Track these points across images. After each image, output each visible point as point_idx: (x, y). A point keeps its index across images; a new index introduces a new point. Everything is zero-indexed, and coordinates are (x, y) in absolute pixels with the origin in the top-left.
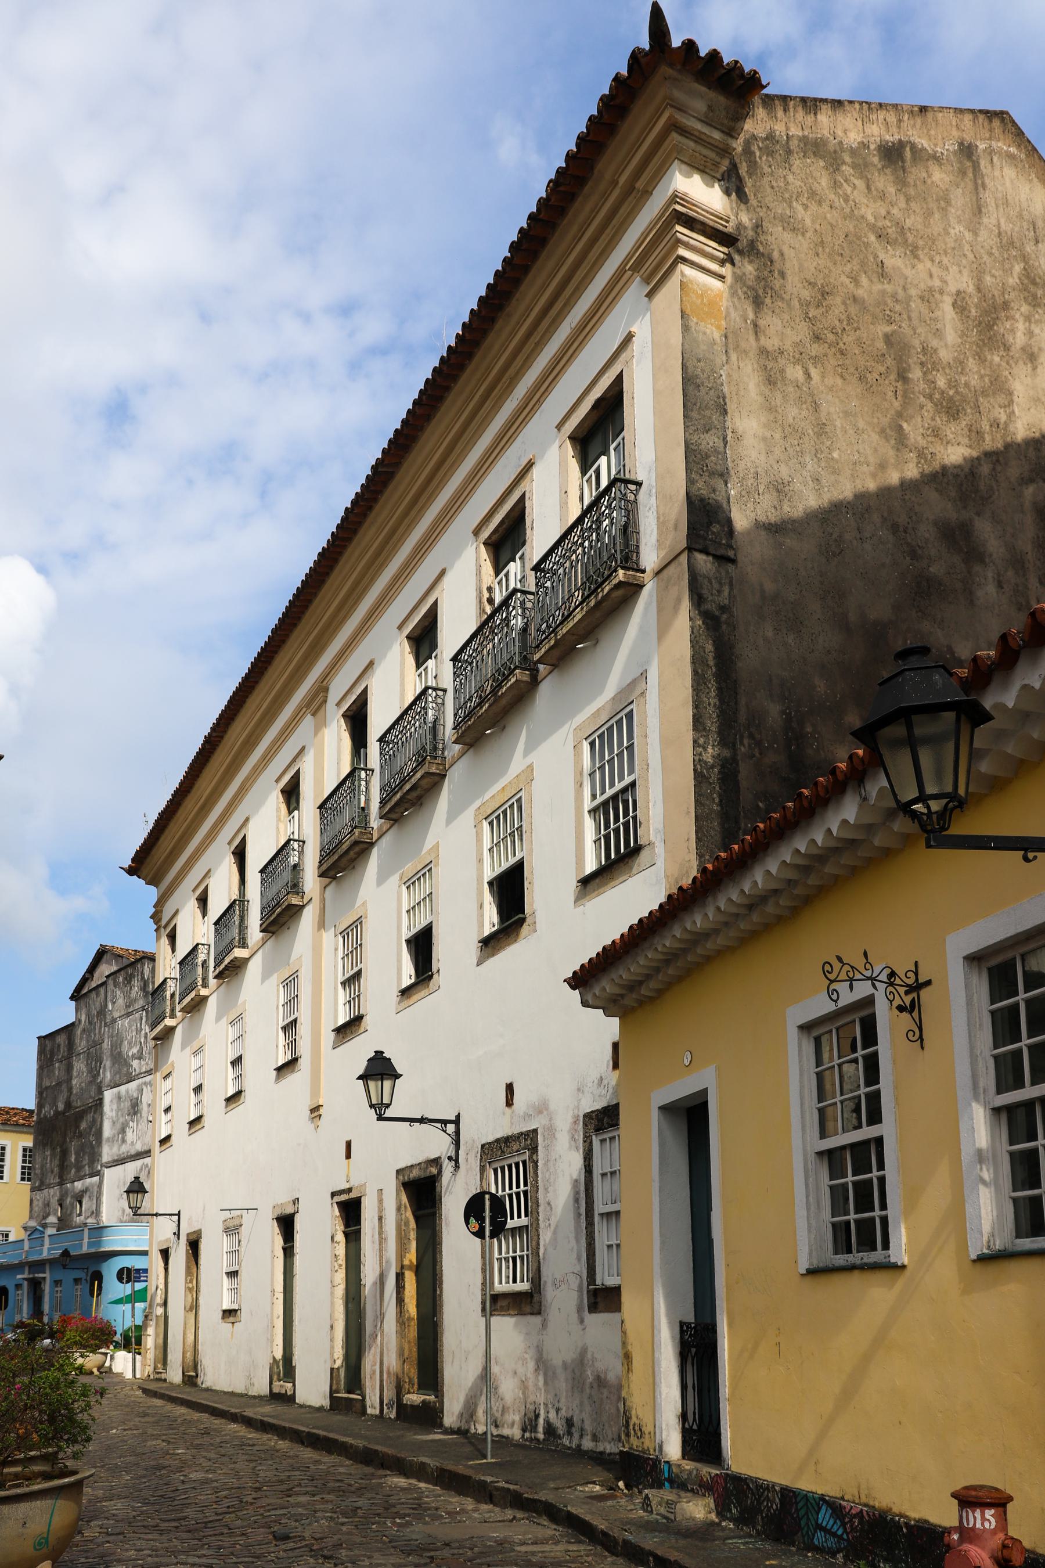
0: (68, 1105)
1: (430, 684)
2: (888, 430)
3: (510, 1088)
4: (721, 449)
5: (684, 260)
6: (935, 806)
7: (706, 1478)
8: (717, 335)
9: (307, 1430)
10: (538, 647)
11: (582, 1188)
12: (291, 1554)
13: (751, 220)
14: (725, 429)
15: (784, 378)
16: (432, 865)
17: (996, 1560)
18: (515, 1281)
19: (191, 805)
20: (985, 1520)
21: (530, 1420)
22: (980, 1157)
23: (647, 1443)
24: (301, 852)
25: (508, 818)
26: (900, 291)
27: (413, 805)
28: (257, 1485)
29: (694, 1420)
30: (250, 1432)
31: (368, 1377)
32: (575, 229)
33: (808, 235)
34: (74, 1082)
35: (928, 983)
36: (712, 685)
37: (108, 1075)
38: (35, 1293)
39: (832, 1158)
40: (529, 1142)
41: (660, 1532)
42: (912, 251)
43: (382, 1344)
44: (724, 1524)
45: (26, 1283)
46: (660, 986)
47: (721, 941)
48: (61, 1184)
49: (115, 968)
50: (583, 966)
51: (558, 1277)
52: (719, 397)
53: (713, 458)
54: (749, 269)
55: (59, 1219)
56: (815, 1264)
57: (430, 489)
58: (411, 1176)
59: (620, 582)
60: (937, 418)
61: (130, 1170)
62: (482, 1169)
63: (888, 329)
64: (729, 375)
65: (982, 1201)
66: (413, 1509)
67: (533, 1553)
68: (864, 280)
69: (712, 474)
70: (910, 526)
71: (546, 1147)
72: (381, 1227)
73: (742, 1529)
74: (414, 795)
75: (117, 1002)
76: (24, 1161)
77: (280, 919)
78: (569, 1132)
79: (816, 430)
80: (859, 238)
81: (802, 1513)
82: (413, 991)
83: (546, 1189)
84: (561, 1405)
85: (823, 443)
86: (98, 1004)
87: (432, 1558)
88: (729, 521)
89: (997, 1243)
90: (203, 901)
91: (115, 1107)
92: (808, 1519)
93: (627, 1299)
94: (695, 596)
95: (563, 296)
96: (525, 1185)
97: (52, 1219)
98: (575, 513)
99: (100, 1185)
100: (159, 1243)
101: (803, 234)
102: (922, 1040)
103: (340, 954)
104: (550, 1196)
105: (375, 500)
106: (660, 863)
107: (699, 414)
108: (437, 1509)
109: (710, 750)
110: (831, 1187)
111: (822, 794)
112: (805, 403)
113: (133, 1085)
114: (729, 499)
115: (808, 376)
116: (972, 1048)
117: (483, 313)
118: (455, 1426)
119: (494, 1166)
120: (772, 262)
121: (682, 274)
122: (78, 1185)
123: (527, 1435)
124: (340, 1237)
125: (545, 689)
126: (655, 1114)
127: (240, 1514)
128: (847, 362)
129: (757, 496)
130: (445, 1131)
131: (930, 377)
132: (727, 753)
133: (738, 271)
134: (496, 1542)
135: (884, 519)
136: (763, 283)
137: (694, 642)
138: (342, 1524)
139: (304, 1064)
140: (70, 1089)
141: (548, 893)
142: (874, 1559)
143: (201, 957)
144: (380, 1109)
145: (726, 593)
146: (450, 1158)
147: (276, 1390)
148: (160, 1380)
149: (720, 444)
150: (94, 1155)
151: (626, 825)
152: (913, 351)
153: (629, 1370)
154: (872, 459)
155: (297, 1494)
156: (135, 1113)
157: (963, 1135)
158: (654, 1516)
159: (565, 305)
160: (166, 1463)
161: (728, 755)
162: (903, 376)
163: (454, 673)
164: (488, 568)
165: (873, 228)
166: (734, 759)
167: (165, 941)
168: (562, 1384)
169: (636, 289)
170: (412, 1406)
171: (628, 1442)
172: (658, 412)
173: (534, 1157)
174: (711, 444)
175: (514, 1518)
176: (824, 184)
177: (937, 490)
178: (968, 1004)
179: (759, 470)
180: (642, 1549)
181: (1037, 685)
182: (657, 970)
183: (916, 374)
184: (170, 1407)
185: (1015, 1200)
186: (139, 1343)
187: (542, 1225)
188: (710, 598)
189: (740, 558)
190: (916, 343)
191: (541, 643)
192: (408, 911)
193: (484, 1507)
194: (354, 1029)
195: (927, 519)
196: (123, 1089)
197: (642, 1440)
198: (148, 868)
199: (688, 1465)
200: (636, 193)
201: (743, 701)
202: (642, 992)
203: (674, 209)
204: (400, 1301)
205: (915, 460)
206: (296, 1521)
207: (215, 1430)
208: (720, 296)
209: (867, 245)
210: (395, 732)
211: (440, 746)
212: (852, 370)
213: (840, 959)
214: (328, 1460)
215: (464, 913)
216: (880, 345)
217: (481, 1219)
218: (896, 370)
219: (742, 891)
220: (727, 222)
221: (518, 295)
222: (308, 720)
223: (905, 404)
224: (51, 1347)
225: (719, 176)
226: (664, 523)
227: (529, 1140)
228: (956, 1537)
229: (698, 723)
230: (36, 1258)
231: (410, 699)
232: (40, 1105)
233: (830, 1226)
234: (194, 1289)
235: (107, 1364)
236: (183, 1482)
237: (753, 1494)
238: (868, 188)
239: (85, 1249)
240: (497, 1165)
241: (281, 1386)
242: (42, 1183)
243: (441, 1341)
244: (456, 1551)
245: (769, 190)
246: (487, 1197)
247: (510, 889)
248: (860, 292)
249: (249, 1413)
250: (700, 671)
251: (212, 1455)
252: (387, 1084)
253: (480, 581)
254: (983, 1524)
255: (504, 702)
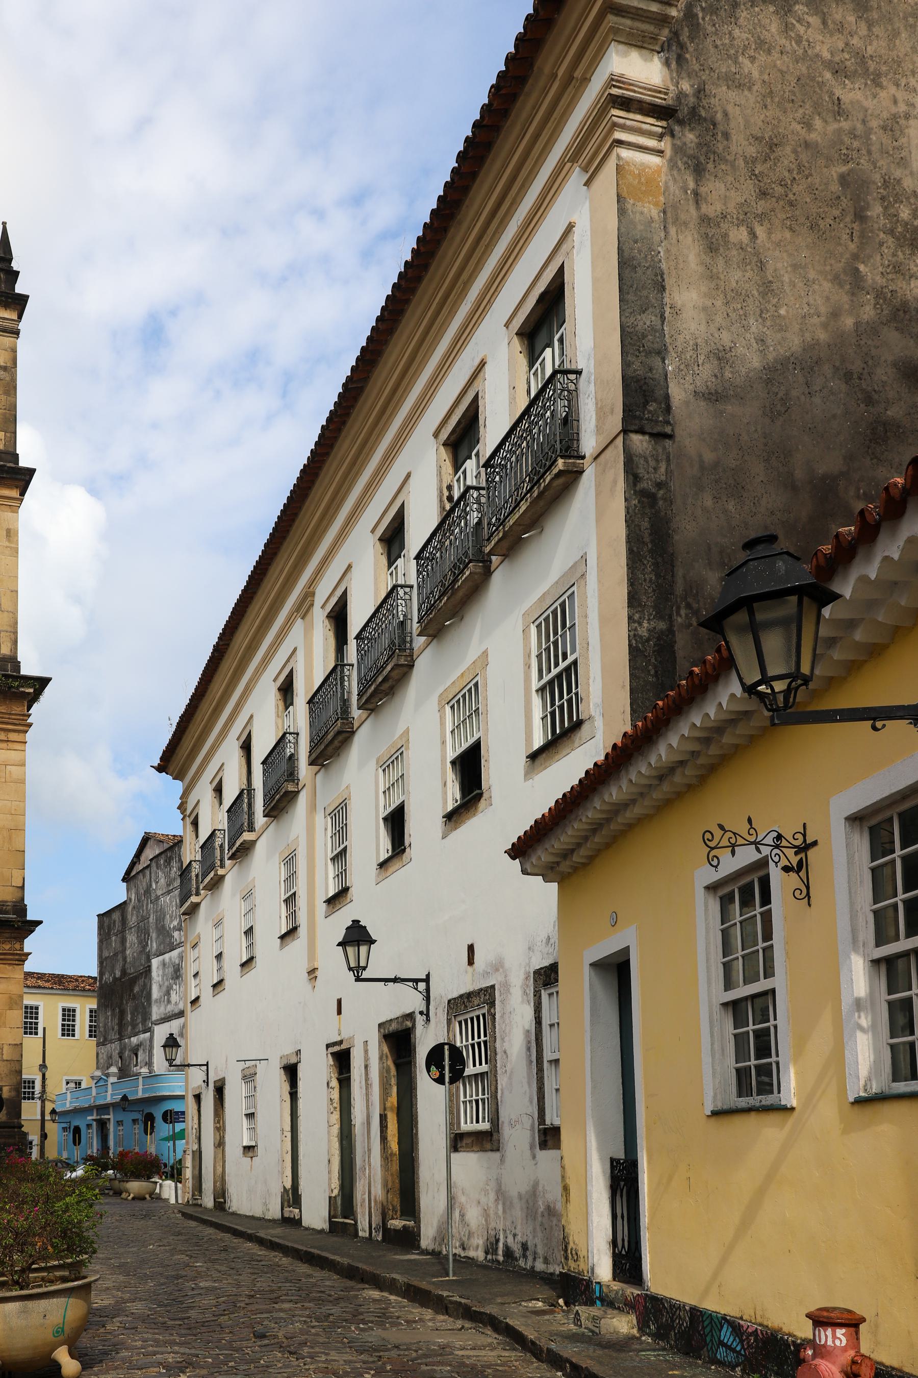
0: (124, 972)
1: (399, 582)
2: (842, 276)
3: (471, 948)
4: (659, 327)
5: (620, 143)
6: (779, 686)
7: (630, 1298)
8: (655, 213)
9: (305, 1249)
10: (488, 539)
11: (533, 1038)
12: (264, 1349)
13: (692, 86)
14: (662, 306)
15: (727, 242)
16: (403, 749)
17: (846, 1373)
18: (477, 1122)
19: (206, 707)
20: (837, 1338)
21: (492, 1244)
22: (858, 1004)
23: (582, 1266)
24: (296, 743)
25: (467, 700)
26: (859, 126)
27: (387, 695)
28: (253, 1293)
29: (623, 1246)
30: (261, 1250)
31: (359, 1204)
32: (518, 127)
33: (755, 88)
34: (128, 952)
35: (815, 843)
36: (648, 562)
37: (154, 945)
38: (102, 1132)
39: (735, 1007)
40: (487, 997)
41: (582, 1343)
42: (873, 80)
43: (370, 1176)
44: (643, 1338)
45: (95, 1123)
46: (590, 854)
47: (637, 811)
48: (120, 1039)
49: (157, 852)
50: (519, 838)
51: (513, 1117)
52: (656, 275)
53: (650, 337)
54: (690, 137)
55: (120, 1069)
56: (719, 1106)
57: (396, 399)
58: (391, 1029)
59: (560, 471)
60: (900, 253)
61: (173, 1027)
62: (449, 1022)
63: (844, 169)
64: (668, 251)
65: (859, 1048)
66: (378, 1317)
67: (469, 1357)
68: (818, 123)
69: (649, 353)
70: (866, 371)
71: (502, 1002)
72: (367, 1074)
73: (658, 1344)
74: (386, 686)
75: (160, 881)
76: (91, 1021)
77: (279, 804)
78: (521, 987)
79: (761, 289)
80: (813, 79)
81: (707, 1330)
82: (390, 864)
83: (503, 1039)
84: (517, 1231)
85: (769, 302)
86: (144, 884)
87: (380, 1357)
88: (667, 397)
89: (874, 1087)
90: (218, 790)
91: (161, 973)
92: (712, 1335)
93: (564, 1135)
94: (631, 477)
95: (509, 196)
96: (485, 1036)
97: (114, 1069)
98: (523, 403)
99: (151, 1039)
100: (193, 1089)
101: (750, 89)
102: (809, 898)
103: (329, 834)
104: (506, 1045)
105: (348, 415)
106: (599, 736)
107: (636, 295)
108: (398, 1318)
109: (645, 624)
110: (735, 1035)
111: (710, 671)
112: (750, 264)
113: (175, 953)
114: (666, 376)
115: (753, 235)
116: (852, 904)
117: (436, 225)
118: (430, 1248)
119: (459, 1018)
120: (714, 125)
121: (618, 156)
122: (134, 1040)
123: (489, 1257)
124: (335, 1083)
125: (497, 578)
126: (587, 969)
127: (232, 1316)
128: (797, 213)
129: (696, 368)
130: (416, 989)
131: (892, 211)
132: (662, 625)
133: (678, 143)
134: (439, 1346)
135: (836, 369)
136: (705, 149)
137: (629, 522)
138: (313, 1327)
139: (302, 931)
140: (125, 959)
141: (502, 769)
142: (766, 1373)
143: (218, 842)
144: (358, 972)
145: (663, 469)
146: (421, 1013)
147: (286, 1215)
148: (196, 1205)
149: (656, 321)
150: (146, 1015)
151: (570, 701)
152: (873, 187)
153: (567, 1201)
154: (823, 310)
155: (283, 1301)
156: (177, 977)
157: (844, 986)
158: (583, 1330)
159: (512, 204)
160: (183, 1273)
161: (665, 627)
162: (860, 216)
163: (418, 571)
164: (448, 467)
165: (828, 65)
166: (670, 631)
167: (189, 828)
168: (518, 1213)
169: (577, 177)
170: (394, 1230)
171: (567, 1264)
172: (596, 300)
173: (492, 1010)
174: (648, 323)
175: (463, 1327)
176: (773, 30)
177: (897, 329)
178: (848, 863)
179: (699, 341)
180: (561, 1357)
181: (896, 556)
182: (586, 838)
183: (876, 210)
184: (201, 1228)
185: (892, 1047)
186: (180, 1173)
187: (499, 1072)
188: (646, 476)
189: (679, 432)
190: (877, 177)
191: (492, 536)
192: (384, 792)
193: (442, 1317)
194: (341, 900)
195: (885, 361)
196: (167, 957)
197: (578, 1263)
198: (174, 765)
199: (616, 1286)
200: (574, 82)
201: (680, 572)
202: (574, 859)
203: (609, 94)
204: (384, 1138)
205: (873, 302)
206: (276, 1323)
207: (233, 1248)
208: (658, 171)
209: (821, 85)
210: (369, 629)
211: (408, 639)
212: (802, 220)
213: (721, 827)
214: (318, 1274)
215: (431, 790)
216: (835, 187)
217: (441, 1067)
218: (852, 210)
219: (650, 764)
220: (666, 94)
221: (467, 202)
222: (299, 624)
223: (861, 246)
224: (113, 1176)
225: (658, 48)
226: (601, 408)
227: (487, 995)
228: (810, 1352)
229: (633, 600)
230: (102, 1102)
231: (383, 595)
232: (101, 973)
233: (734, 1071)
234: (220, 1129)
235: (157, 1191)
236: (193, 1289)
237: (667, 1312)
238: (824, 23)
239: (140, 1095)
240: (461, 1018)
241: (290, 1211)
242: (105, 1039)
243: (418, 1174)
244: (402, 1353)
245: (712, 50)
246: (446, 1047)
247: (469, 766)
248: (813, 136)
249: (262, 1234)
250: (635, 549)
251: (223, 1268)
252: (363, 949)
253: (441, 481)
254: (833, 1342)
255: (460, 594)
